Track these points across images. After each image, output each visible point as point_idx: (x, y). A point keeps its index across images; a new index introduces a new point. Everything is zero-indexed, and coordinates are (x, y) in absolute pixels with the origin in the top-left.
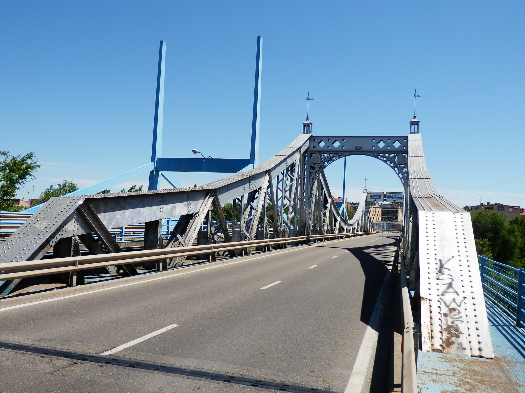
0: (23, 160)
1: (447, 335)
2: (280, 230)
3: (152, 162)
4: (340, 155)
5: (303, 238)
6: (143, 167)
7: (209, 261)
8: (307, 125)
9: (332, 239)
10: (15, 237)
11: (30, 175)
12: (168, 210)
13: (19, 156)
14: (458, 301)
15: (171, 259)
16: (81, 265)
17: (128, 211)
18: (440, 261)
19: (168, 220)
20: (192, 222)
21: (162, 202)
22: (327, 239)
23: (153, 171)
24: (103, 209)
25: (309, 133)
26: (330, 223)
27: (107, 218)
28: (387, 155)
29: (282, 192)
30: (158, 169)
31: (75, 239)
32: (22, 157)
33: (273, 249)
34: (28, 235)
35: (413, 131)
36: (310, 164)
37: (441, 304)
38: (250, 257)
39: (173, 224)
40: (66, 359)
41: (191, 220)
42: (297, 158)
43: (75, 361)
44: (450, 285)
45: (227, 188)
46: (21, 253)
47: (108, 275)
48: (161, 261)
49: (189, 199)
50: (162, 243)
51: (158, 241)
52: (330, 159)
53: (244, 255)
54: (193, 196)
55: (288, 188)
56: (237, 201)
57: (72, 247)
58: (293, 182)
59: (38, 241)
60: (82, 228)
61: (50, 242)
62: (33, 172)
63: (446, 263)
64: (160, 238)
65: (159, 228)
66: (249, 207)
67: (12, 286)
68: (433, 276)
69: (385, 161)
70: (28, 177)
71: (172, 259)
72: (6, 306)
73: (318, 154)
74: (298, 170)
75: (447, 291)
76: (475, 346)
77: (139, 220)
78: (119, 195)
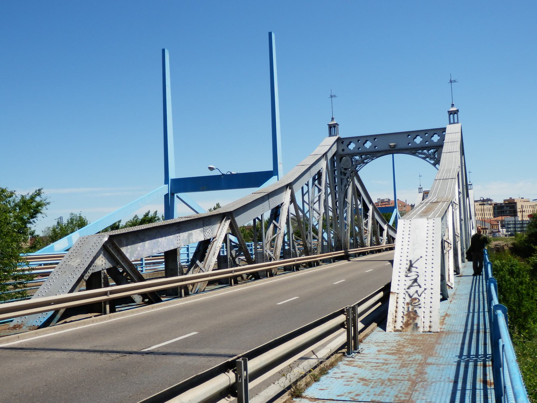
0: (32, 198)
1: (407, 319)
2: (311, 247)
3: (165, 184)
4: (373, 156)
5: (341, 253)
6: (157, 191)
7: (231, 285)
8: (332, 126)
9: (379, 251)
10: (55, 275)
11: (41, 213)
12: (185, 238)
13: (28, 194)
14: (419, 293)
15: (193, 284)
16: (112, 295)
17: (147, 242)
18: (411, 261)
19: (188, 247)
20: (210, 248)
21: (178, 231)
22: (372, 252)
23: (167, 195)
24: (125, 243)
25: (336, 135)
26: (374, 233)
27: (129, 251)
28: (425, 151)
29: (308, 204)
30: (173, 192)
31: (104, 272)
32: (31, 194)
33: (303, 269)
34: (65, 272)
35: (452, 121)
36: (340, 169)
37: (406, 296)
38: (276, 278)
39: (192, 251)
40: (118, 354)
41: (209, 245)
42: (323, 165)
43: (124, 355)
44: (415, 281)
45: (244, 209)
46: (62, 287)
47: (134, 304)
48: (183, 288)
49: (205, 224)
50: (182, 270)
51: (178, 269)
52: (362, 162)
53: (269, 277)
54: (209, 222)
55: (317, 199)
56: (257, 220)
57: (102, 280)
58: (320, 193)
59: (75, 277)
60: (109, 262)
61: (84, 276)
62: (44, 210)
63: (414, 263)
64: (180, 266)
65: (178, 256)
66: (272, 226)
67: (58, 316)
68: (403, 274)
69: (424, 158)
70: (39, 215)
71: (194, 284)
72: (58, 331)
73: (348, 158)
74: (326, 176)
75: (412, 285)
76: (427, 324)
77: (159, 251)
78: (138, 228)
